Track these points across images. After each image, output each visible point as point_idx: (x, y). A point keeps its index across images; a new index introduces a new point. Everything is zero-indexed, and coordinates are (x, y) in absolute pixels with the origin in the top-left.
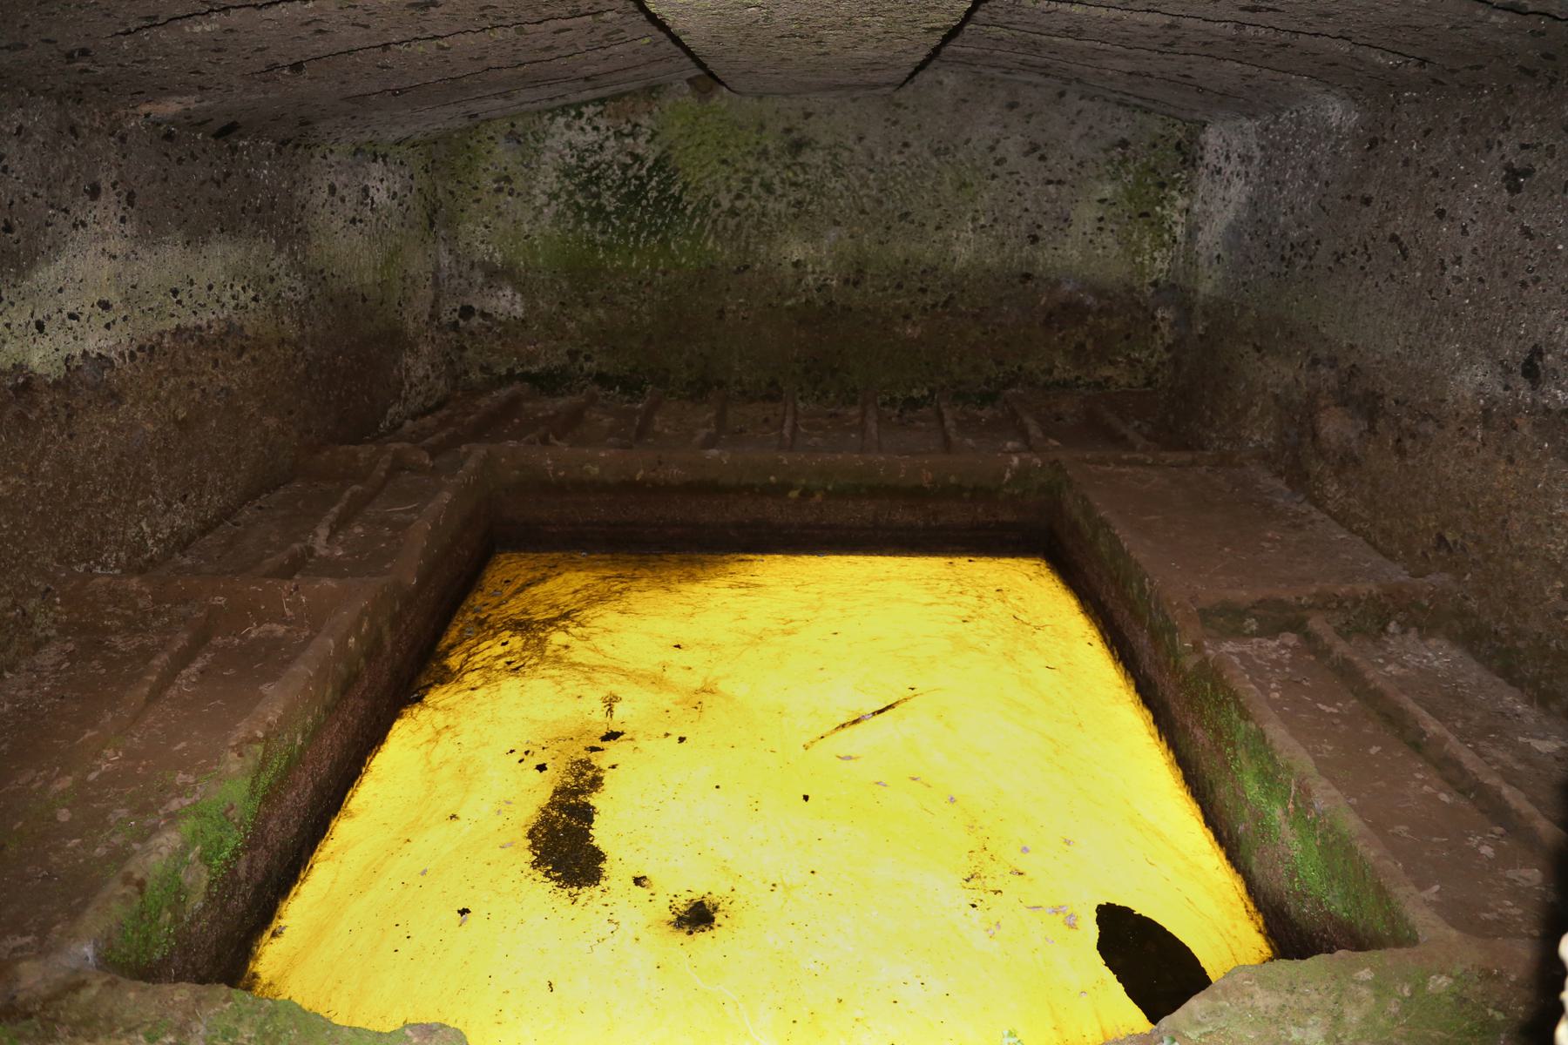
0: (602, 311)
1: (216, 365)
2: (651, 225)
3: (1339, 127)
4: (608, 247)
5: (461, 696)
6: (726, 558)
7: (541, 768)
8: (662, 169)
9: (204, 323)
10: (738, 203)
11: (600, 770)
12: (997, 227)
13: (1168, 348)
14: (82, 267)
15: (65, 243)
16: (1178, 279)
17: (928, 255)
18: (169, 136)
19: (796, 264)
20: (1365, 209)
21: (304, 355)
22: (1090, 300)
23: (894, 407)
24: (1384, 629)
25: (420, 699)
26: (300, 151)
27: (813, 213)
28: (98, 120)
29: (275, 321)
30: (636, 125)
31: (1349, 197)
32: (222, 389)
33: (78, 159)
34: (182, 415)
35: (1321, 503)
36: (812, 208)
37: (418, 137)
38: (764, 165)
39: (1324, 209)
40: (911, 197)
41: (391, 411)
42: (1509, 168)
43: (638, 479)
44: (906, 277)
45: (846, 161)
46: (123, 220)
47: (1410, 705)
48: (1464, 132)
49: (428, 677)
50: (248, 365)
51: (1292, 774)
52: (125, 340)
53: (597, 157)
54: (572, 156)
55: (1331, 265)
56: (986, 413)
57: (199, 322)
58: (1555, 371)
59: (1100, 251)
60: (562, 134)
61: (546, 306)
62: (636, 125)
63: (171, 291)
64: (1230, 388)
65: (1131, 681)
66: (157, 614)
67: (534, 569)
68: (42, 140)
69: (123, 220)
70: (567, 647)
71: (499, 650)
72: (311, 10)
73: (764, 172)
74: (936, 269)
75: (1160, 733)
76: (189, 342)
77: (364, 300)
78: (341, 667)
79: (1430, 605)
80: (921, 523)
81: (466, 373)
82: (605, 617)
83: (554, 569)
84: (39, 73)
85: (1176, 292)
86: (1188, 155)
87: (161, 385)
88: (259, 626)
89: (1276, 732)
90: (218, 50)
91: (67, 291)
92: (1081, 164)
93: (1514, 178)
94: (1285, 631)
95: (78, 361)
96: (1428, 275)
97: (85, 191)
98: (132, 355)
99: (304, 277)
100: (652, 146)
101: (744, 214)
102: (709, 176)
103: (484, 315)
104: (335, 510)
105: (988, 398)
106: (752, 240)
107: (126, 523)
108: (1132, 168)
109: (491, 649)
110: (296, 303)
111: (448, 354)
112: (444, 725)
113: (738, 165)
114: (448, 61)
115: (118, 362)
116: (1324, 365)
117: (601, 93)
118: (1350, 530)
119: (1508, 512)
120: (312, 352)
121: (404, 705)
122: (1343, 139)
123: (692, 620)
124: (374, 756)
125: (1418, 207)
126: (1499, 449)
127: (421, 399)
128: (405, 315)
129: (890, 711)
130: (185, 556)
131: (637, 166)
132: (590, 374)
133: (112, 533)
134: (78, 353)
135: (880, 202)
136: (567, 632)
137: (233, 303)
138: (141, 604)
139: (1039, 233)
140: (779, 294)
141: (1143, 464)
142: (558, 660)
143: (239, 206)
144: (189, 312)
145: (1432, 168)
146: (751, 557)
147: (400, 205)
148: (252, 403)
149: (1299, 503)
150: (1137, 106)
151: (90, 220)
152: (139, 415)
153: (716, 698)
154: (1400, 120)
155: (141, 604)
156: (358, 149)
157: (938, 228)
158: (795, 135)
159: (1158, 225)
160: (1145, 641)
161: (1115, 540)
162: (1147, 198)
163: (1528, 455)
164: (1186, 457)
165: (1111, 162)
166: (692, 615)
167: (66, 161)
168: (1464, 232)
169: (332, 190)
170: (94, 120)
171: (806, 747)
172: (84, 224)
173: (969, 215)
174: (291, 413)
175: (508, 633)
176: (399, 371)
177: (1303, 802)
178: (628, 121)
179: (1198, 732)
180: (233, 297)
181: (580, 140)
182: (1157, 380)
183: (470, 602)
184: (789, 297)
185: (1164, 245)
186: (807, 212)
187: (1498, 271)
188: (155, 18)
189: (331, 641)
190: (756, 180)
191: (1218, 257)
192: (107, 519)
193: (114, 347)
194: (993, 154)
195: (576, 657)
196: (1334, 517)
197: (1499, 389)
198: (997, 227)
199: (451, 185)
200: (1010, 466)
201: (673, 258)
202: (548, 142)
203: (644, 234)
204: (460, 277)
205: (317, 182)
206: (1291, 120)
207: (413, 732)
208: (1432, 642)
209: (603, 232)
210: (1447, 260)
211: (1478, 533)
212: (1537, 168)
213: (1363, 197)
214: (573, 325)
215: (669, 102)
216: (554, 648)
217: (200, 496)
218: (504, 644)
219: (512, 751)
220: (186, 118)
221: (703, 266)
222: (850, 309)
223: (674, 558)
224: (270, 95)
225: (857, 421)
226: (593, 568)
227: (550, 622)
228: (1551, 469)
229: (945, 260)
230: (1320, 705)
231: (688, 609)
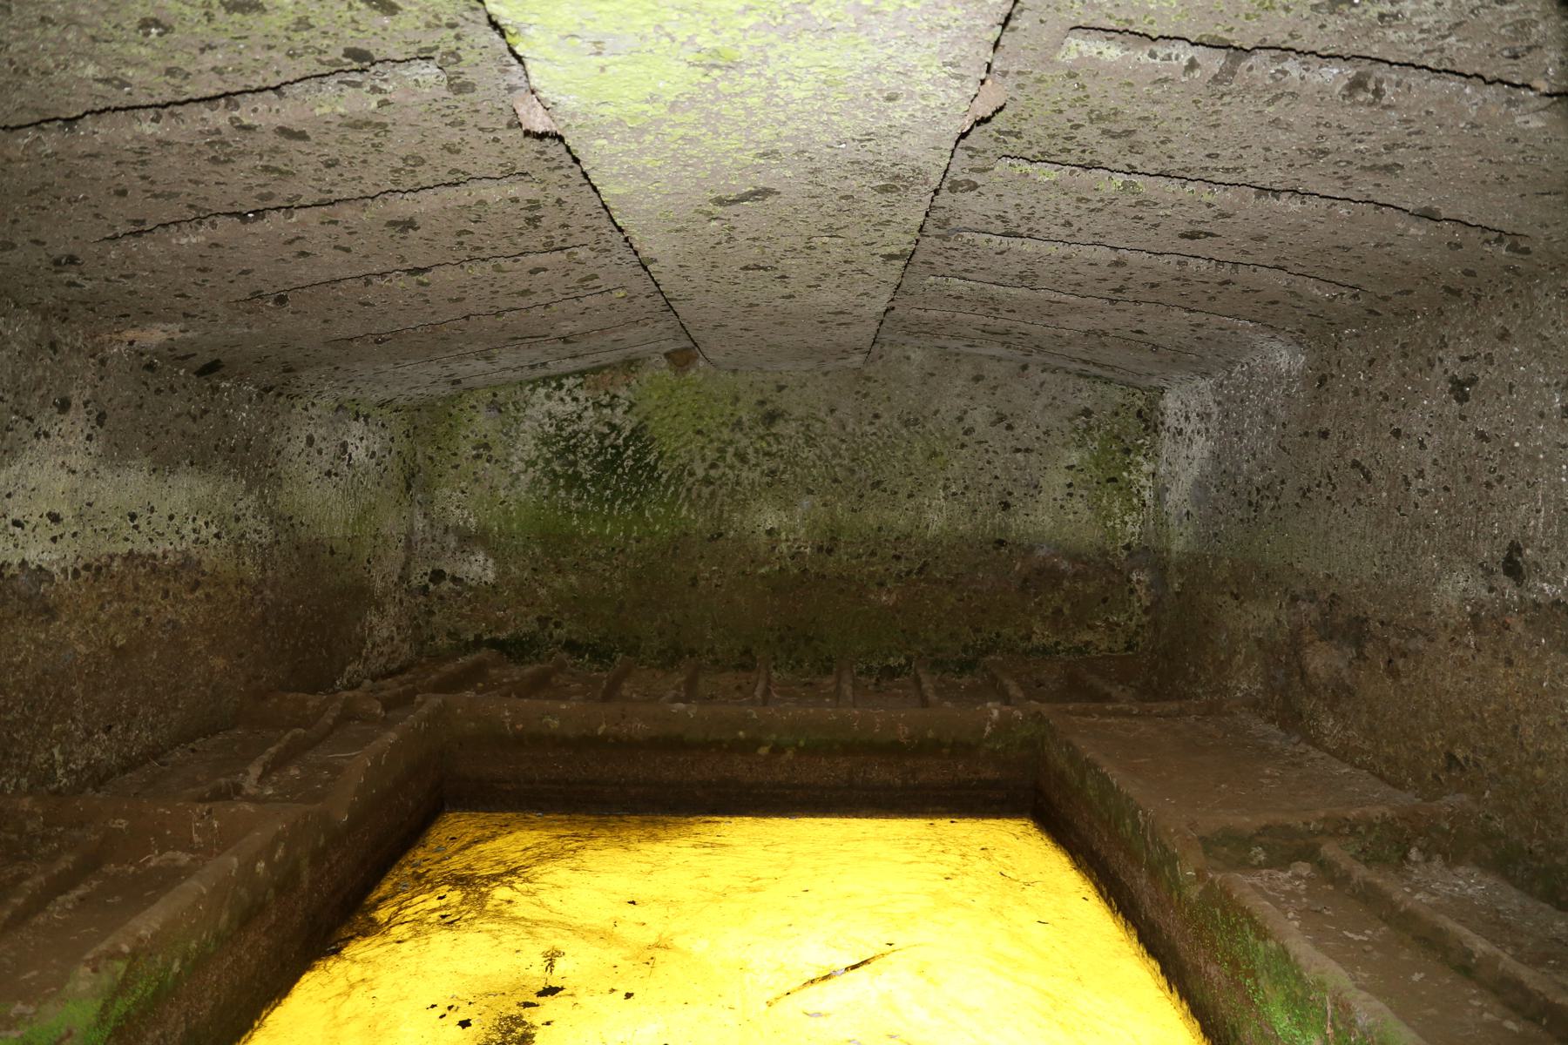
0: (574, 577)
1: (166, 594)
2: (626, 493)
3: (1288, 372)
4: (583, 514)
5: (384, 949)
6: (691, 819)
7: (465, 1024)
8: (639, 438)
9: (160, 553)
10: (712, 472)
11: (533, 1027)
12: (968, 494)
13: (1146, 611)
14: (36, 477)
15: (23, 450)
16: (1150, 541)
17: (900, 522)
18: (150, 367)
19: (770, 532)
20: (1323, 443)
21: (262, 599)
22: (1065, 565)
23: (871, 677)
24: (1405, 857)
25: (337, 952)
26: (282, 400)
27: (787, 482)
28: (80, 339)
29: (235, 561)
30: (614, 397)
31: (1306, 434)
32: (169, 621)
33: (52, 372)
34: (121, 641)
35: (1318, 741)
36: (785, 477)
37: (401, 401)
38: (739, 435)
39: (1284, 449)
40: (883, 465)
41: (348, 668)
42: (1453, 380)
43: (600, 733)
44: (880, 545)
45: (818, 431)
46: (89, 438)
47: (1450, 924)
48: (1405, 355)
49: (350, 928)
50: (201, 601)
51: (1325, 991)
52: (71, 556)
53: (576, 427)
54: (551, 425)
55: (1298, 501)
56: (966, 680)
57: (154, 551)
58: (1536, 564)
59: (1071, 517)
60: (543, 404)
61: (517, 571)
62: (614, 397)
63: (129, 515)
64: (1212, 641)
65: (1133, 932)
66: (45, 839)
67: (483, 828)
68: (18, 348)
69: (89, 438)
70: (510, 902)
71: (435, 903)
72: (294, 225)
73: (738, 442)
74: (909, 536)
75: (1169, 983)
76: (141, 569)
77: (332, 552)
78: (243, 892)
79: (1452, 828)
80: (898, 781)
81: (433, 638)
82: (557, 873)
83: (506, 827)
84: (26, 282)
85: (1150, 555)
86: (1149, 421)
87: (102, 608)
88: (161, 853)
89: (1300, 947)
90: (204, 270)
91: (15, 497)
92: (1047, 433)
93: (1460, 389)
94: (1296, 860)
95: (14, 570)
96: (1394, 493)
97: (54, 403)
98: (76, 573)
99: (271, 522)
100: (629, 416)
101: (719, 482)
102: (685, 445)
103: (455, 579)
104: (272, 750)
105: (965, 666)
106: (726, 508)
107: (35, 746)
108: (1097, 436)
109: (427, 902)
110: (260, 546)
111: (415, 618)
112: (360, 978)
113: (713, 436)
114: (427, 301)
115: (59, 578)
116: (1304, 600)
117: (582, 364)
118: (1353, 764)
119: (1518, 717)
120: (272, 597)
121: (319, 958)
122: (1294, 382)
123: (650, 877)
124: (272, 1010)
125: (1374, 430)
126: (1495, 652)
127: (383, 660)
128: (374, 572)
129: (864, 967)
130: (98, 792)
131: (613, 435)
132: (559, 642)
133: (16, 756)
134: (16, 561)
135: (852, 471)
136: (511, 887)
137: (193, 537)
138: (30, 826)
139: (1010, 500)
140: (753, 561)
141: (1128, 714)
142: (498, 915)
143: (212, 443)
144: (145, 538)
145: (1381, 393)
146: (717, 819)
147: (378, 464)
148: (200, 639)
149: (1295, 745)
150: (1097, 377)
151: (53, 432)
152: (73, 635)
153: (671, 954)
154: (1345, 355)
155: (30, 826)
156: (340, 406)
157: (910, 496)
158: (769, 407)
159: (1126, 490)
160: (1144, 881)
161: (1105, 779)
162: (1113, 464)
163: (1527, 654)
164: (1174, 706)
165: (1076, 429)
166: (650, 873)
167: (40, 372)
168: (1422, 446)
169: (310, 441)
170: (77, 340)
171: (769, 1004)
172: (47, 435)
173: (941, 483)
174: (241, 656)
175: (447, 887)
176: (362, 628)
177: (1343, 1022)
178: (607, 393)
179: (1212, 970)
180: (194, 531)
181: (559, 409)
182: (1137, 644)
183: (410, 857)
184: (763, 565)
185: (1134, 509)
186: (781, 481)
187: (1461, 477)
188: (143, 222)
189: (235, 860)
190: (731, 450)
191: (1188, 513)
192: (14, 739)
193: (58, 561)
194: (961, 425)
195: (518, 911)
196: (1333, 753)
197: (1484, 592)
198: (968, 494)
199: (430, 451)
200: (990, 719)
201: (647, 525)
202: (528, 412)
203: (619, 502)
204: (434, 541)
205: (295, 431)
206: (1242, 373)
207: (323, 986)
208: (1461, 870)
209: (578, 499)
210: (1409, 475)
211: (1489, 744)
212: (1479, 376)
213: (1319, 432)
214: (544, 591)
215: (648, 375)
216: (495, 902)
217: (127, 729)
218: (440, 898)
219: (433, 1006)
220: (170, 350)
221: (677, 534)
222: (824, 577)
223: (635, 819)
224: (255, 331)
225: (832, 689)
226: (547, 828)
227: (495, 878)
228: (1554, 665)
229: (918, 527)
230: (1346, 933)
231: (647, 867)
